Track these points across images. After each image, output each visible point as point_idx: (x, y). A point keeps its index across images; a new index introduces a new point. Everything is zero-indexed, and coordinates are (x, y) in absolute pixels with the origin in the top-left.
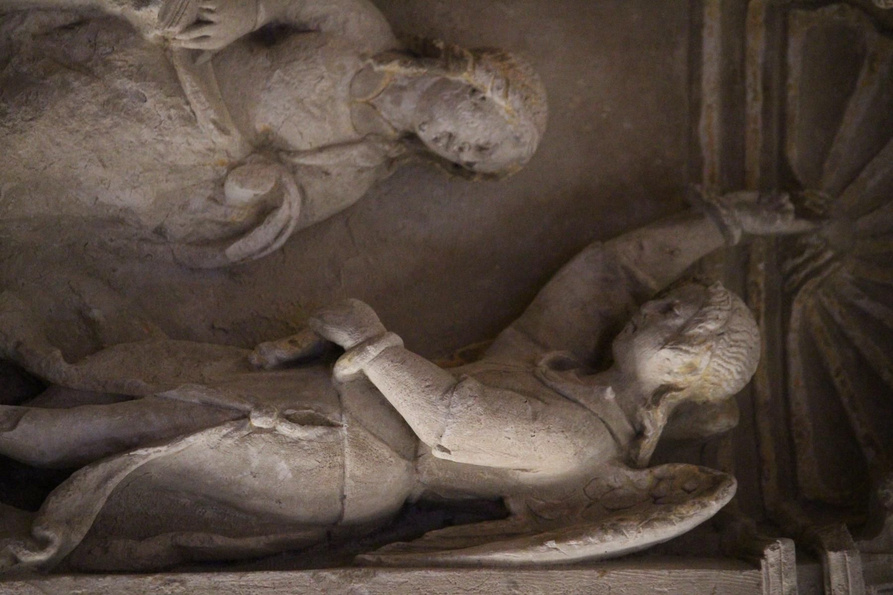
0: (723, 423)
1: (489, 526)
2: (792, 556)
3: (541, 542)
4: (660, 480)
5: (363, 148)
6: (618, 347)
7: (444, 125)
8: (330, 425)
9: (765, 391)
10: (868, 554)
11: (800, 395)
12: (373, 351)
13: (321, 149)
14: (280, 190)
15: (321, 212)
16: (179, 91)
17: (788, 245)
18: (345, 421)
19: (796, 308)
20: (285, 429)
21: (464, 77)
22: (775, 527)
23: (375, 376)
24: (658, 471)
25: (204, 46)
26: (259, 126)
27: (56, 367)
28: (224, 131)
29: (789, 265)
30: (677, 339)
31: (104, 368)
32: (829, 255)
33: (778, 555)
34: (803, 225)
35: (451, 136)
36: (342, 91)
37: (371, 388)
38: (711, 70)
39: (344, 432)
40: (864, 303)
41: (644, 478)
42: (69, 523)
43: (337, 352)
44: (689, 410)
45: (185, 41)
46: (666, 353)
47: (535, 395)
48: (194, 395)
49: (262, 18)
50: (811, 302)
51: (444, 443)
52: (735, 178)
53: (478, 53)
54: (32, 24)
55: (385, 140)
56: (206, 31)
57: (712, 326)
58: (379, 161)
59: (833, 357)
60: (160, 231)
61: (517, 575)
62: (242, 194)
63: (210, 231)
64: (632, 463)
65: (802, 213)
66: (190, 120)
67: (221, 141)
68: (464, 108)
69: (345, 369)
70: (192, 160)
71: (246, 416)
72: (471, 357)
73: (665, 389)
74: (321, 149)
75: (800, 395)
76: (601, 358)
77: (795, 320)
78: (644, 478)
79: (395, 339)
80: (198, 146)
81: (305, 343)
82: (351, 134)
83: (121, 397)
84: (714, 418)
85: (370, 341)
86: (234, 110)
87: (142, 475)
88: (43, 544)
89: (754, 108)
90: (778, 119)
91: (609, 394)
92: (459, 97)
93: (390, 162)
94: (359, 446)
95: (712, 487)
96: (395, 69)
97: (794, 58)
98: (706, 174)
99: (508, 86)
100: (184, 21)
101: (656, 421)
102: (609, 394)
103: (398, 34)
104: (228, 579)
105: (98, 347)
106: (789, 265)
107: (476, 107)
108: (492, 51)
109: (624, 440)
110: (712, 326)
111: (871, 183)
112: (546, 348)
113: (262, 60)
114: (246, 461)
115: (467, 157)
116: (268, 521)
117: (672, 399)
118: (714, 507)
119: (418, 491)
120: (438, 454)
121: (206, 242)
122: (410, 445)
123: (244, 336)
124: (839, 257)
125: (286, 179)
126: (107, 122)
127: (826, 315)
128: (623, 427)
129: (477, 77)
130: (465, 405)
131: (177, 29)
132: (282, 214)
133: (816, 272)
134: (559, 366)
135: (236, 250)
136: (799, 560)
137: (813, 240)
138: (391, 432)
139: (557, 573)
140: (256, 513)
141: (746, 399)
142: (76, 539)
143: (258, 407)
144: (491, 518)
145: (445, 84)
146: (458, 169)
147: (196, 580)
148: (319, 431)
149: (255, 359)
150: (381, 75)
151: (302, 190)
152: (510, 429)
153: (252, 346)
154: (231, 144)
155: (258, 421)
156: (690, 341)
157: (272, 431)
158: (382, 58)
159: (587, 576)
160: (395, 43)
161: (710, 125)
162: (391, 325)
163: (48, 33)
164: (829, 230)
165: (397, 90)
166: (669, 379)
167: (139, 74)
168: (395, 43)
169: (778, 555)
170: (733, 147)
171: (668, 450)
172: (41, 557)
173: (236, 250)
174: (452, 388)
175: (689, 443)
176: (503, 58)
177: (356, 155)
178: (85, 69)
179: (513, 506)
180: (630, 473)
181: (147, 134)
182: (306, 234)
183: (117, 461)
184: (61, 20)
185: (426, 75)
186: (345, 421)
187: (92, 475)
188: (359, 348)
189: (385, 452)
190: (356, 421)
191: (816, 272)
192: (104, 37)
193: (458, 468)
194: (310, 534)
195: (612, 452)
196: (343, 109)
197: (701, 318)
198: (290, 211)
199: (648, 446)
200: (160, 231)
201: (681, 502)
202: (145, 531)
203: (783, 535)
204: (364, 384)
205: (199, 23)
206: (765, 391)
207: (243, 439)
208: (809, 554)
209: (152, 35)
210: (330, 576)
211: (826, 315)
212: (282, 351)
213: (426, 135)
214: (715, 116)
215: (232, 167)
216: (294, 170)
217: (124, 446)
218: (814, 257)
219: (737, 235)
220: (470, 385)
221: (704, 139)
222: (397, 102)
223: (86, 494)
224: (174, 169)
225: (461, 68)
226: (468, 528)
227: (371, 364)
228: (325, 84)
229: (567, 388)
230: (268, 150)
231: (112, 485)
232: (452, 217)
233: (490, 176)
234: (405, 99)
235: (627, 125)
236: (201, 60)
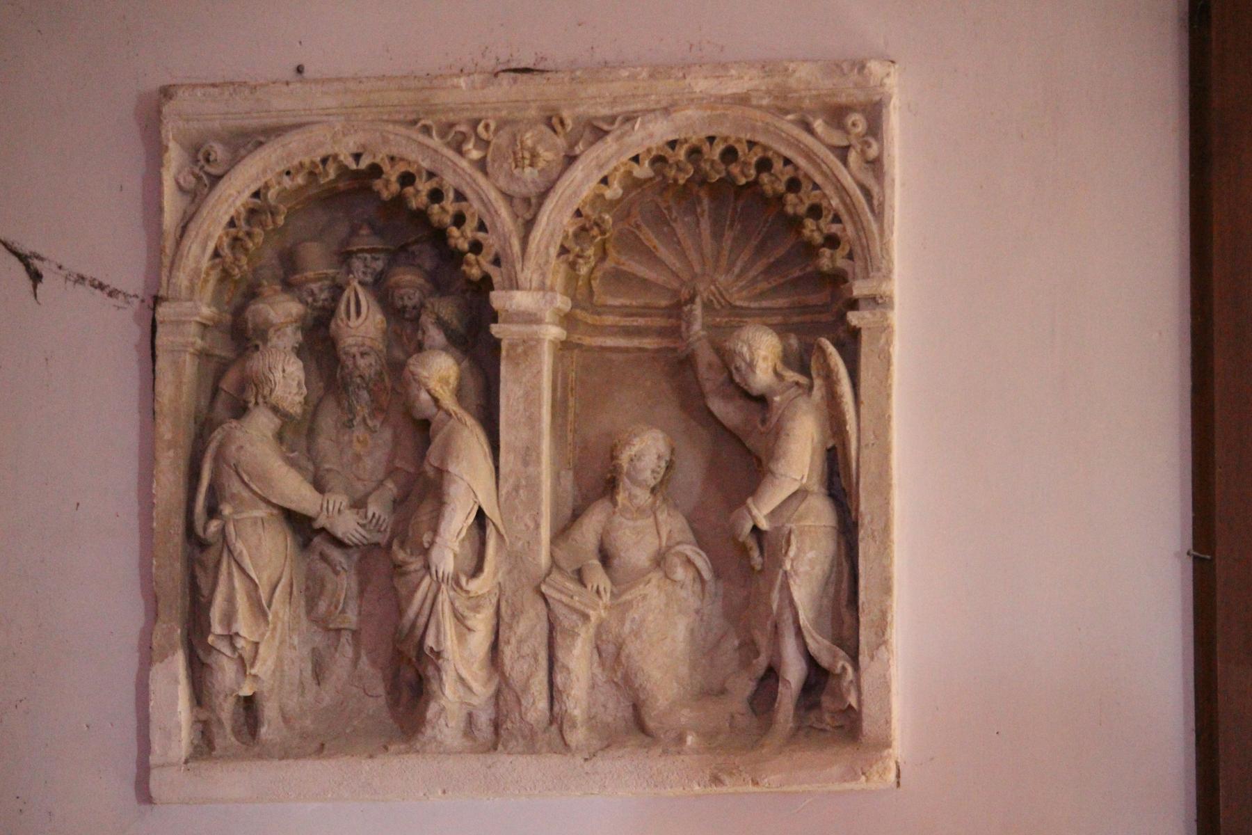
0: (794, 341)
1: (839, 457)
2: (856, 313)
3: (847, 432)
4: (819, 375)
5: (658, 513)
6: (755, 393)
7: (648, 474)
8: (790, 533)
9: (778, 319)
10: (855, 278)
11: (781, 302)
12: (755, 512)
13: (658, 533)
14: (678, 554)
15: (690, 536)
16: (630, 602)
17: (708, 306)
18: (789, 525)
19: (738, 303)
20: (792, 554)
21: (625, 466)
22: (842, 318)
23: (767, 510)
24: (814, 375)
25: (608, 590)
26: (647, 564)
27: (762, 662)
28: (649, 582)
29: (718, 307)
30: (751, 366)
31: (762, 641)
32: (712, 287)
33: (853, 318)
34: (698, 300)
35: (653, 471)
36: (631, 523)
37: (773, 513)
38: (622, 342)
39: (793, 526)
40: (737, 270)
41: (818, 383)
42: (835, 656)
43: (755, 529)
44: (787, 359)
45: (606, 598)
46: (758, 371)
47: (776, 434)
48: (775, 596)
49: (596, 562)
50: (736, 296)
51: (799, 478)
52: (674, 332)
53: (613, 458)
54: (598, 671)
55: (654, 503)
56: (601, 589)
57: (745, 349)
58: (664, 506)
59: (763, 285)
60: (697, 612)
61: (863, 444)
62: (680, 573)
63: (698, 587)
64: (811, 388)
65: (692, 300)
66: (644, 597)
67: (654, 582)
68: (640, 465)
69: (764, 525)
70: (662, 595)
71: (786, 572)
72: (759, 461)
73: (777, 374)
74: (658, 533)
75: (781, 302)
76: (762, 401)
77: (745, 304)
78: (818, 383)
79: (750, 501)
80: (656, 593)
81: (752, 543)
82: (651, 519)
83: (776, 631)
84: (790, 345)
85: (750, 513)
86: (639, 576)
87: (816, 623)
88: (844, 668)
89: (641, 322)
90: (644, 311)
91: (777, 399)
92: (634, 468)
93: (665, 500)
94: (800, 518)
95: (822, 351)
96: (621, 498)
97: (617, 302)
98: (672, 345)
99: (628, 443)
100: (597, 599)
101: (792, 376)
102: (777, 399)
103: (602, 495)
104: (862, 582)
105: (753, 642)
106: (718, 307)
107: (639, 459)
108: (612, 451)
109: (800, 391)
110: (745, 349)
111: (678, 265)
112: (755, 427)
113: (616, 562)
114: (807, 573)
115: (663, 464)
116: (836, 564)
117: (780, 368)
118: (831, 349)
119: (823, 490)
120: (804, 481)
121: (703, 590)
122: (800, 494)
123: (749, 572)
124: (713, 282)
125: (673, 551)
126: (645, 636)
127: (741, 289)
128: (793, 391)
129: (624, 459)
130: (781, 467)
131: (601, 603)
132: (690, 553)
133: (721, 294)
134: (764, 421)
135: (707, 575)
136: (857, 309)
137: (705, 295)
138: (795, 502)
139: (862, 425)
140: (832, 566)
141: (782, 330)
142: (842, 653)
143: (781, 567)
144: (835, 455)
145: (628, 474)
146: (670, 466)
147: (862, 597)
148: (793, 537)
149: (758, 567)
150: (624, 505)
151: (678, 543)
152: (793, 447)
153: (753, 569)
154: (656, 577)
155: (788, 566)
156: (752, 360)
157: (793, 560)
158: (615, 504)
159: (863, 410)
160: (608, 497)
161: (649, 343)
162: (743, 503)
163: (602, 664)
164: (701, 287)
165: (631, 497)
166: (770, 370)
167: (622, 621)
168: (608, 497)
169: (853, 318)
170: (661, 332)
171: (804, 370)
172: (850, 670)
173: (707, 575)
174: (772, 473)
175: (800, 360)
176: (616, 445)
177: (662, 517)
178: (620, 648)
179: (830, 445)
180: (815, 388)
181: (651, 618)
182: (701, 543)
183: (806, 634)
184: (596, 657)
185: (625, 482)
186: (789, 525)
187: (813, 646)
188: (754, 518)
189: (803, 506)
190: (788, 520)
191: (721, 294)
192: (604, 637)
193: (811, 470)
194: (843, 543)
195: (805, 397)
196: (639, 523)
197: (741, 355)
198: (690, 550)
199: (803, 380)
200: (697, 612)
201: (829, 365)
202: (837, 620)
203: (845, 314)
204: (772, 515)
205: (598, 592)
206: (778, 319)
207: (796, 574)
208: (854, 304)
209: (604, 614)
210: (861, 533)
211: (741, 289)
212: (755, 554)
213: (652, 483)
214: (642, 268)
215: (666, 576)
216: (669, 548)
217: (799, 632)
218: (714, 295)
219: (702, 333)
220: (772, 466)
221: (656, 346)
222: (636, 497)
223: (819, 645)
224: (667, 605)
225: (621, 466)
226: (841, 466)
227: (761, 512)
228: (628, 532)
229: (774, 420)
230: (660, 561)
231: (815, 634)
232: (692, 472)
233: (673, 451)
234: (634, 494)
235: (648, 383)
236: (615, 590)
